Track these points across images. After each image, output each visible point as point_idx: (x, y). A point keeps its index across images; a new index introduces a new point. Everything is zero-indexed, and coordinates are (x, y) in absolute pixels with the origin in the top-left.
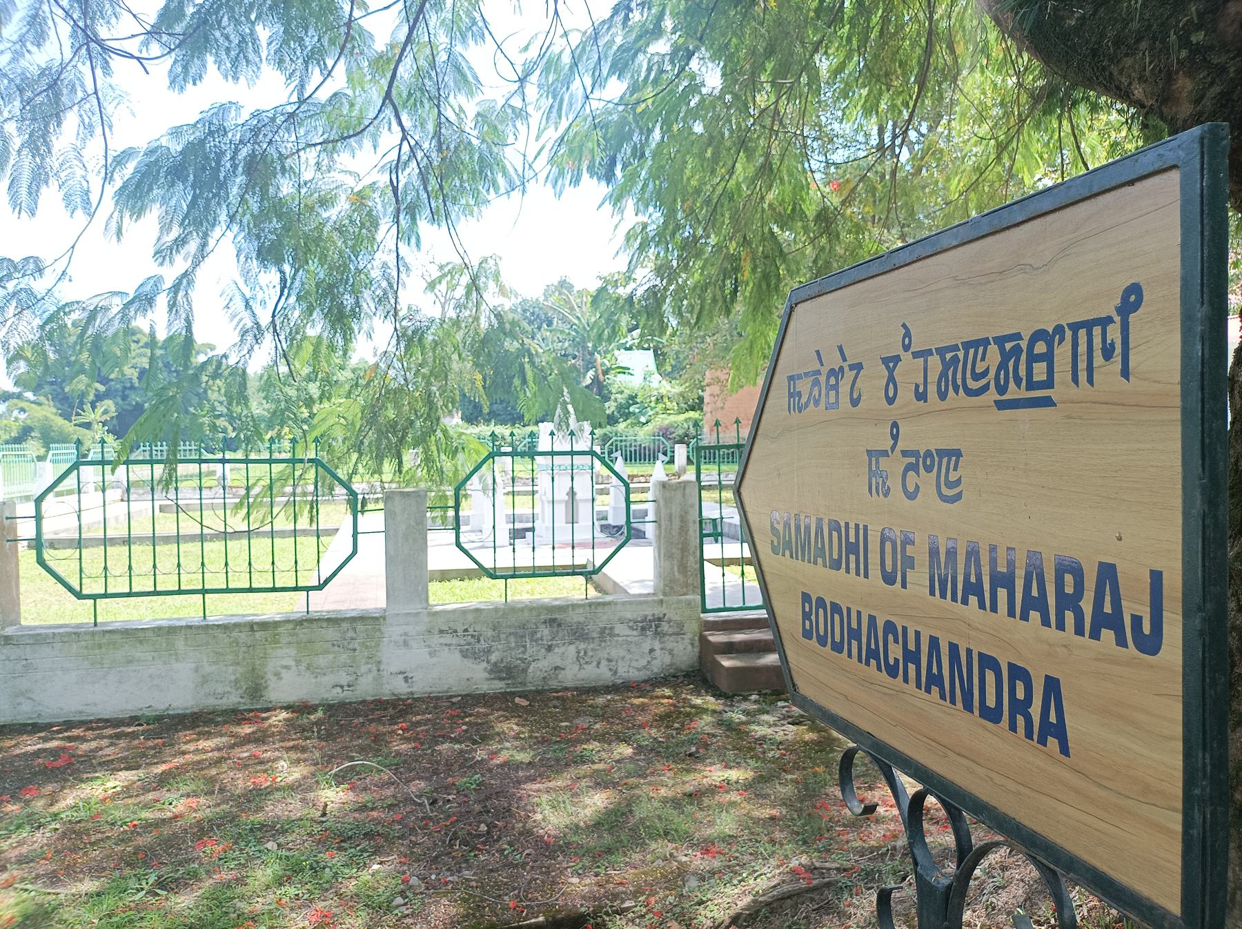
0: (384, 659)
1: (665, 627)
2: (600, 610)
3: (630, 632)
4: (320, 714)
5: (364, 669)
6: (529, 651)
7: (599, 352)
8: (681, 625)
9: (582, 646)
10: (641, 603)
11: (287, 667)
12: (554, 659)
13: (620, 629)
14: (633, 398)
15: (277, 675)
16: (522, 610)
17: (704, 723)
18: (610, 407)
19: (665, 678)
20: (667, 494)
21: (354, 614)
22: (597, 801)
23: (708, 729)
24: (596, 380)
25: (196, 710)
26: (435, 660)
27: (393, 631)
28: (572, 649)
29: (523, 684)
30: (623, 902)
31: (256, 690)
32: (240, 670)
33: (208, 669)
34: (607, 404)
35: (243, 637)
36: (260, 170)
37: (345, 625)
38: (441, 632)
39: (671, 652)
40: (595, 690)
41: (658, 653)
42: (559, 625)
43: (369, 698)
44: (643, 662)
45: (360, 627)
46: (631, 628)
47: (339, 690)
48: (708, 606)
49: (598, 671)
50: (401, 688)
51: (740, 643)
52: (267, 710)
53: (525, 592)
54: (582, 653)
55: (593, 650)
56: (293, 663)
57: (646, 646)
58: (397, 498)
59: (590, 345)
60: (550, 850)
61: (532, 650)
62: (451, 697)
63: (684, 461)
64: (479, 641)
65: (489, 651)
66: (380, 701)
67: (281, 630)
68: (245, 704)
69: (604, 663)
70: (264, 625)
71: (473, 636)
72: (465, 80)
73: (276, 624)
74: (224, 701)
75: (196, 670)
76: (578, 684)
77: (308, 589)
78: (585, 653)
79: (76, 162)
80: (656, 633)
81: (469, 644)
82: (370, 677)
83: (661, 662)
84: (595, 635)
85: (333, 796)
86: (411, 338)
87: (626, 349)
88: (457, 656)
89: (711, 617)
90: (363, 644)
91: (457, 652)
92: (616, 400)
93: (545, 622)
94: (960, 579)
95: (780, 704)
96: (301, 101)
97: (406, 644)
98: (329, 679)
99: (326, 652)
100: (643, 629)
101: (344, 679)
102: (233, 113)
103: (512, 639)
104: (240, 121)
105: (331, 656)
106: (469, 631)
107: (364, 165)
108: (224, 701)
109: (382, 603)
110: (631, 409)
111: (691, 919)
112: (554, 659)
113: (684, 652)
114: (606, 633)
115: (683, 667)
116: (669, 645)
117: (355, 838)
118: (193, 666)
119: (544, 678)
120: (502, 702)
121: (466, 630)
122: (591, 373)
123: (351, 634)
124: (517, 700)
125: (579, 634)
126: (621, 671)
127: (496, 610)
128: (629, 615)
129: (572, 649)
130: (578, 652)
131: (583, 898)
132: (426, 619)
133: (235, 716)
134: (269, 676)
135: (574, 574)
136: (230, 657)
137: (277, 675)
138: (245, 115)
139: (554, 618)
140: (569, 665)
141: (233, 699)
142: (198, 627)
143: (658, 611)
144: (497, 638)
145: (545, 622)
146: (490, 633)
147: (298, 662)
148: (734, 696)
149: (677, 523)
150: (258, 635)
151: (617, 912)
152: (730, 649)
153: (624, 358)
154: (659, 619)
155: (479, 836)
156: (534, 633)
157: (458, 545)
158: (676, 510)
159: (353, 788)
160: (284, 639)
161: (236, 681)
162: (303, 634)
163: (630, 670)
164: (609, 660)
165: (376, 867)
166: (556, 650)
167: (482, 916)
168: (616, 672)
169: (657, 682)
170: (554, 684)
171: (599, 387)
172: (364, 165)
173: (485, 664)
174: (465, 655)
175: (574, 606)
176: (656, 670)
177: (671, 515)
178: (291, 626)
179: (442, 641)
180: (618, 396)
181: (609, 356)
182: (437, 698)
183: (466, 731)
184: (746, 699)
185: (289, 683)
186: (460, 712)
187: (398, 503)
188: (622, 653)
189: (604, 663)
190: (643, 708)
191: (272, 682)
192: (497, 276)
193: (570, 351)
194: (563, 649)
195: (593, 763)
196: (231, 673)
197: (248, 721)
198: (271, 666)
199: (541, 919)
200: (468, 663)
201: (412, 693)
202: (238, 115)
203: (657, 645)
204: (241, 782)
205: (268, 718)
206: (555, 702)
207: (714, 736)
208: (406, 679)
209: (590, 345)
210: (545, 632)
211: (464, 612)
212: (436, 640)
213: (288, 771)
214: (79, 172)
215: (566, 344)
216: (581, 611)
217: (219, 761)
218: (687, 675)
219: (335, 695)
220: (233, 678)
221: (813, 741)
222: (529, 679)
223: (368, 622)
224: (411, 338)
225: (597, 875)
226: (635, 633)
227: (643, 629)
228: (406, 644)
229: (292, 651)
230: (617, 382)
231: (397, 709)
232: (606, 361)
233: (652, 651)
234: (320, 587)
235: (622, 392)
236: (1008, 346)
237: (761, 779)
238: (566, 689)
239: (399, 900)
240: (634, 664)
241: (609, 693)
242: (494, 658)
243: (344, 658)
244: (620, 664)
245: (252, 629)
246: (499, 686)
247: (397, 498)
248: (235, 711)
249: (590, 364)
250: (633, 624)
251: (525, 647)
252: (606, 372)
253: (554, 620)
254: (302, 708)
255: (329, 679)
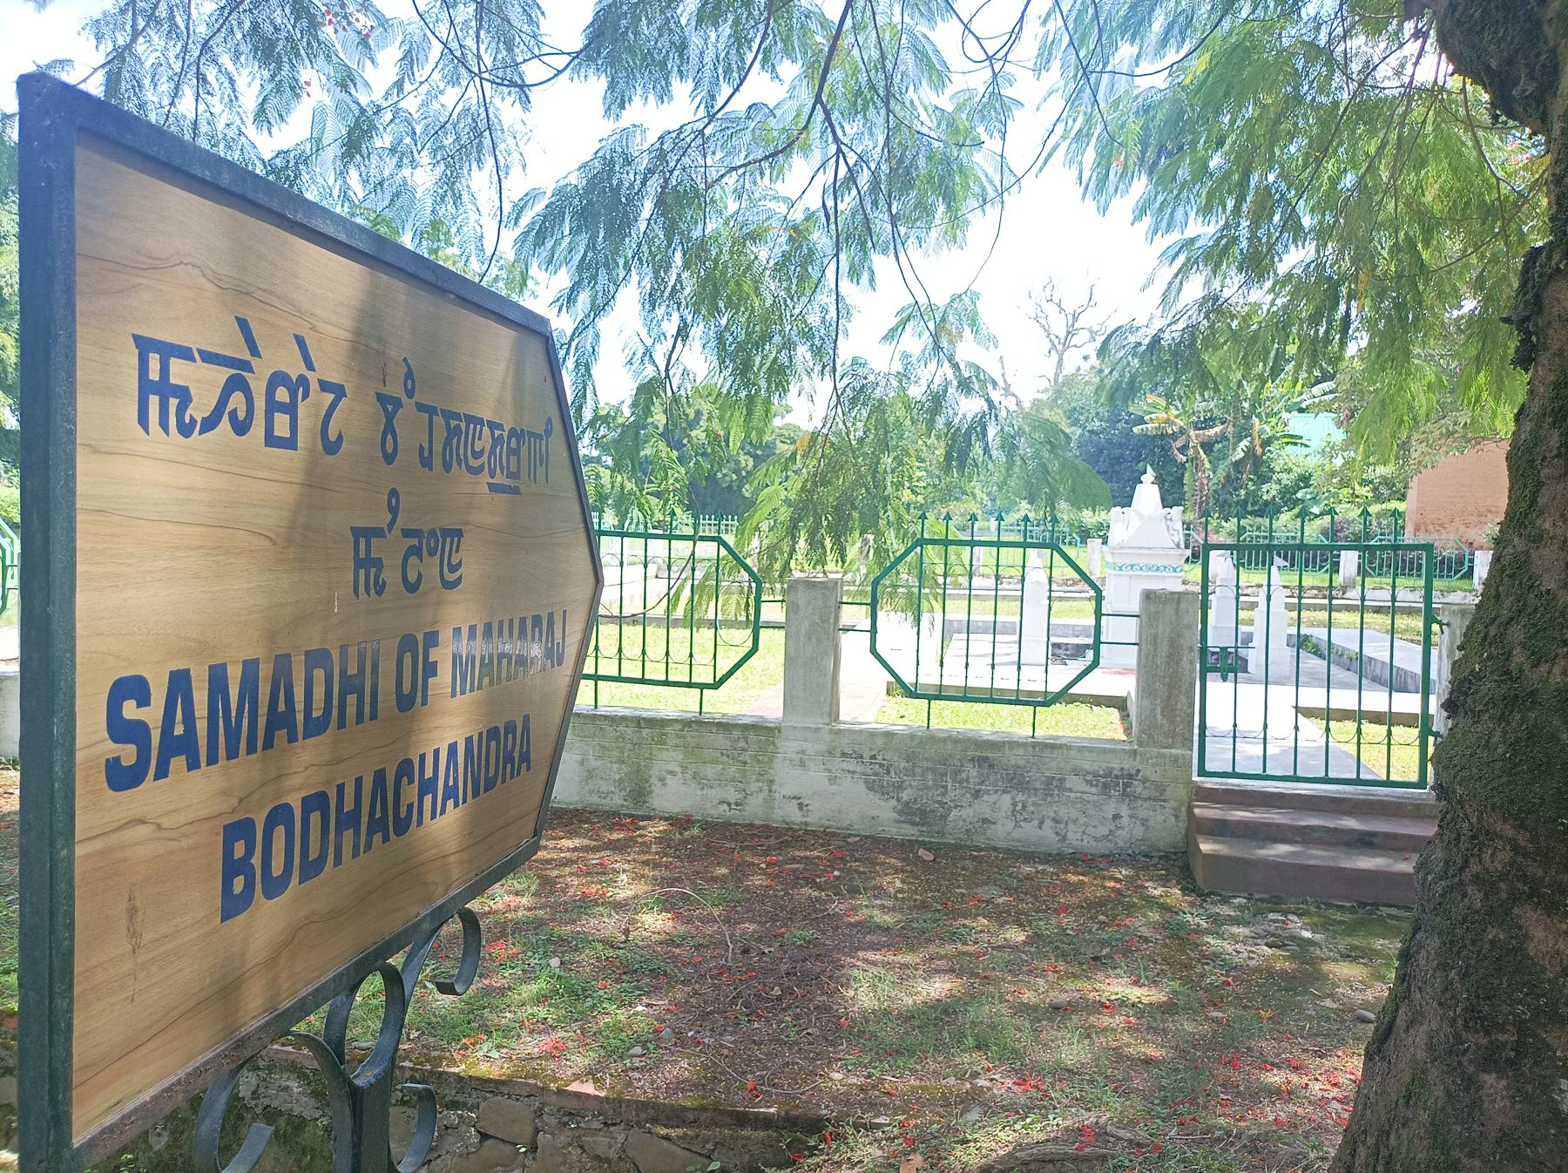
0: (777, 780)
1: (1137, 787)
2: (1046, 754)
3: (1087, 789)
4: (695, 831)
5: (754, 786)
6: (951, 794)
7: (1259, 416)
8: (1161, 788)
9: (1020, 797)
10: (1105, 751)
11: (671, 773)
12: (981, 808)
13: (1073, 782)
14: (1305, 480)
15: (662, 779)
16: (944, 740)
17: (1144, 923)
18: (1270, 491)
19: (1133, 857)
20: (1152, 608)
21: (747, 721)
22: (939, 988)
23: (1145, 931)
24: (1250, 452)
25: (579, 806)
26: (835, 787)
27: (789, 747)
28: (1006, 799)
29: (941, 834)
30: (876, 1116)
31: (640, 793)
32: (625, 769)
33: (594, 763)
34: (1265, 487)
35: (629, 732)
36: (680, 203)
37: (736, 733)
38: (844, 755)
39: (1144, 822)
40: (1029, 857)
41: (1125, 821)
42: (991, 766)
43: (758, 822)
44: (1105, 831)
45: (752, 737)
46: (1089, 783)
47: (726, 807)
48: (1209, 767)
49: (1040, 833)
50: (795, 815)
51: (1238, 822)
52: (649, 818)
53: (952, 718)
54: (1020, 806)
55: (1034, 804)
56: (678, 769)
57: (1110, 810)
58: (801, 588)
59: (1246, 405)
60: (839, 1030)
61: (953, 793)
62: (850, 835)
63: (1354, 570)
64: (888, 773)
65: (900, 787)
66: (768, 827)
67: (668, 729)
68: (628, 808)
69: (1048, 823)
70: (652, 723)
71: (881, 765)
72: (936, 72)
73: (664, 722)
74: (608, 801)
75: (582, 763)
76: (1012, 845)
77: (702, 687)
78: (1024, 807)
79: (470, 206)
80: (1124, 794)
81: (876, 774)
82: (761, 797)
83: (1129, 832)
84: (1038, 785)
85: (655, 922)
86: (856, 395)
87: (1301, 410)
88: (861, 788)
89: (1210, 783)
90: (755, 758)
91: (861, 783)
92: (1279, 481)
93: (973, 760)
94: (263, 710)
95: (1271, 916)
96: (711, 118)
97: (802, 764)
98: (716, 793)
99: (714, 761)
100: (1105, 786)
101: (732, 796)
102: (638, 139)
103: (930, 776)
104: (646, 146)
105: (719, 767)
106: (880, 757)
107: (801, 184)
108: (608, 801)
109: (780, 714)
110: (1299, 495)
111: (940, 1158)
112: (981, 808)
113: (1163, 825)
114: (1055, 785)
115: (1161, 845)
116: (1143, 814)
117: (639, 971)
118: (579, 758)
119: (968, 831)
120: (905, 848)
121: (873, 757)
122: (1244, 443)
123: (742, 744)
124: (921, 852)
125: (1016, 781)
126: (1073, 837)
127: (912, 736)
128: (1086, 766)
129: (1006, 799)
130: (1015, 804)
131: (834, 1099)
132: (827, 737)
133: (613, 819)
134: (654, 780)
135: (1018, 702)
136: (615, 753)
137: (662, 779)
138: (652, 137)
139: (984, 755)
140: (999, 817)
141: (616, 801)
142: (586, 716)
143: (1129, 765)
144: (910, 772)
145: (973, 760)
146: (903, 764)
147: (684, 768)
148: (1209, 894)
149: (1163, 650)
150: (645, 732)
151: (864, 1126)
152: (1219, 829)
153: (1297, 424)
154: (1130, 776)
155: (768, 1000)
156: (957, 772)
157: (873, 651)
158: (1164, 630)
159: (677, 916)
160: (672, 741)
161: (621, 781)
162: (691, 736)
163: (1084, 837)
164: (1056, 821)
165: (640, 1008)
166: (986, 798)
167: (712, 1090)
168: (1064, 838)
169: (1113, 859)
170: (980, 840)
171: (1257, 465)
172: (801, 184)
173: (894, 802)
174: (871, 787)
175: (1013, 745)
176: (1121, 844)
177: (1156, 636)
178: (678, 727)
179: (844, 766)
180: (1284, 476)
181: (1274, 420)
182: (834, 835)
183: (837, 878)
184: (1225, 901)
185: (674, 793)
186: (844, 854)
187: (802, 596)
188: (1074, 814)
189: (1048, 823)
190: (1074, 888)
191: (656, 787)
192: (973, 322)
193: (1217, 413)
194: (994, 798)
195: (965, 943)
196: (616, 771)
197: (620, 827)
198: (657, 769)
199: (772, 1110)
200: (874, 798)
201: (806, 824)
202: (644, 140)
203: (1124, 811)
204: (575, 885)
205: (644, 828)
206: (968, 863)
207: (1146, 940)
208: (801, 806)
209: (1246, 405)
210: (973, 772)
211: (873, 734)
212: (837, 764)
213: (625, 887)
214: (473, 216)
215: (1212, 405)
216: (1021, 751)
217: (570, 862)
218: (1165, 857)
219: (720, 812)
220: (617, 777)
221: (1284, 972)
222: (949, 828)
223: (759, 733)
224: (856, 395)
225: (869, 1077)
226: (1094, 790)
227: (1105, 786)
228: (802, 764)
229: (678, 755)
230: (1287, 459)
231: (784, 837)
232: (1268, 429)
233: (1116, 817)
234: (716, 685)
235: (1289, 471)
236: (453, 423)
237: (1168, 1009)
238: (995, 849)
239: (638, 1050)
240: (1090, 830)
241: (1041, 863)
242: (905, 796)
243: (733, 770)
244: (1071, 827)
245: (639, 726)
246: (910, 832)
247: (801, 588)
248: (615, 814)
249: (1244, 431)
250: (1092, 778)
251: (945, 787)
252: (1267, 443)
253: (985, 759)
254: (681, 822)
255: (716, 793)
